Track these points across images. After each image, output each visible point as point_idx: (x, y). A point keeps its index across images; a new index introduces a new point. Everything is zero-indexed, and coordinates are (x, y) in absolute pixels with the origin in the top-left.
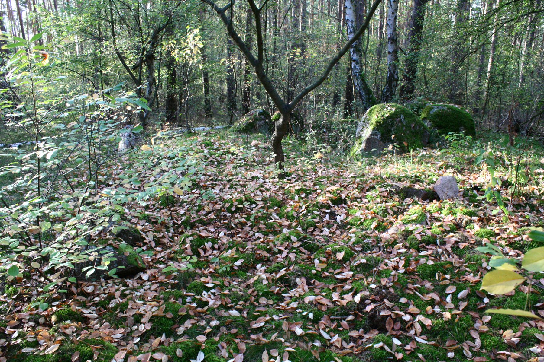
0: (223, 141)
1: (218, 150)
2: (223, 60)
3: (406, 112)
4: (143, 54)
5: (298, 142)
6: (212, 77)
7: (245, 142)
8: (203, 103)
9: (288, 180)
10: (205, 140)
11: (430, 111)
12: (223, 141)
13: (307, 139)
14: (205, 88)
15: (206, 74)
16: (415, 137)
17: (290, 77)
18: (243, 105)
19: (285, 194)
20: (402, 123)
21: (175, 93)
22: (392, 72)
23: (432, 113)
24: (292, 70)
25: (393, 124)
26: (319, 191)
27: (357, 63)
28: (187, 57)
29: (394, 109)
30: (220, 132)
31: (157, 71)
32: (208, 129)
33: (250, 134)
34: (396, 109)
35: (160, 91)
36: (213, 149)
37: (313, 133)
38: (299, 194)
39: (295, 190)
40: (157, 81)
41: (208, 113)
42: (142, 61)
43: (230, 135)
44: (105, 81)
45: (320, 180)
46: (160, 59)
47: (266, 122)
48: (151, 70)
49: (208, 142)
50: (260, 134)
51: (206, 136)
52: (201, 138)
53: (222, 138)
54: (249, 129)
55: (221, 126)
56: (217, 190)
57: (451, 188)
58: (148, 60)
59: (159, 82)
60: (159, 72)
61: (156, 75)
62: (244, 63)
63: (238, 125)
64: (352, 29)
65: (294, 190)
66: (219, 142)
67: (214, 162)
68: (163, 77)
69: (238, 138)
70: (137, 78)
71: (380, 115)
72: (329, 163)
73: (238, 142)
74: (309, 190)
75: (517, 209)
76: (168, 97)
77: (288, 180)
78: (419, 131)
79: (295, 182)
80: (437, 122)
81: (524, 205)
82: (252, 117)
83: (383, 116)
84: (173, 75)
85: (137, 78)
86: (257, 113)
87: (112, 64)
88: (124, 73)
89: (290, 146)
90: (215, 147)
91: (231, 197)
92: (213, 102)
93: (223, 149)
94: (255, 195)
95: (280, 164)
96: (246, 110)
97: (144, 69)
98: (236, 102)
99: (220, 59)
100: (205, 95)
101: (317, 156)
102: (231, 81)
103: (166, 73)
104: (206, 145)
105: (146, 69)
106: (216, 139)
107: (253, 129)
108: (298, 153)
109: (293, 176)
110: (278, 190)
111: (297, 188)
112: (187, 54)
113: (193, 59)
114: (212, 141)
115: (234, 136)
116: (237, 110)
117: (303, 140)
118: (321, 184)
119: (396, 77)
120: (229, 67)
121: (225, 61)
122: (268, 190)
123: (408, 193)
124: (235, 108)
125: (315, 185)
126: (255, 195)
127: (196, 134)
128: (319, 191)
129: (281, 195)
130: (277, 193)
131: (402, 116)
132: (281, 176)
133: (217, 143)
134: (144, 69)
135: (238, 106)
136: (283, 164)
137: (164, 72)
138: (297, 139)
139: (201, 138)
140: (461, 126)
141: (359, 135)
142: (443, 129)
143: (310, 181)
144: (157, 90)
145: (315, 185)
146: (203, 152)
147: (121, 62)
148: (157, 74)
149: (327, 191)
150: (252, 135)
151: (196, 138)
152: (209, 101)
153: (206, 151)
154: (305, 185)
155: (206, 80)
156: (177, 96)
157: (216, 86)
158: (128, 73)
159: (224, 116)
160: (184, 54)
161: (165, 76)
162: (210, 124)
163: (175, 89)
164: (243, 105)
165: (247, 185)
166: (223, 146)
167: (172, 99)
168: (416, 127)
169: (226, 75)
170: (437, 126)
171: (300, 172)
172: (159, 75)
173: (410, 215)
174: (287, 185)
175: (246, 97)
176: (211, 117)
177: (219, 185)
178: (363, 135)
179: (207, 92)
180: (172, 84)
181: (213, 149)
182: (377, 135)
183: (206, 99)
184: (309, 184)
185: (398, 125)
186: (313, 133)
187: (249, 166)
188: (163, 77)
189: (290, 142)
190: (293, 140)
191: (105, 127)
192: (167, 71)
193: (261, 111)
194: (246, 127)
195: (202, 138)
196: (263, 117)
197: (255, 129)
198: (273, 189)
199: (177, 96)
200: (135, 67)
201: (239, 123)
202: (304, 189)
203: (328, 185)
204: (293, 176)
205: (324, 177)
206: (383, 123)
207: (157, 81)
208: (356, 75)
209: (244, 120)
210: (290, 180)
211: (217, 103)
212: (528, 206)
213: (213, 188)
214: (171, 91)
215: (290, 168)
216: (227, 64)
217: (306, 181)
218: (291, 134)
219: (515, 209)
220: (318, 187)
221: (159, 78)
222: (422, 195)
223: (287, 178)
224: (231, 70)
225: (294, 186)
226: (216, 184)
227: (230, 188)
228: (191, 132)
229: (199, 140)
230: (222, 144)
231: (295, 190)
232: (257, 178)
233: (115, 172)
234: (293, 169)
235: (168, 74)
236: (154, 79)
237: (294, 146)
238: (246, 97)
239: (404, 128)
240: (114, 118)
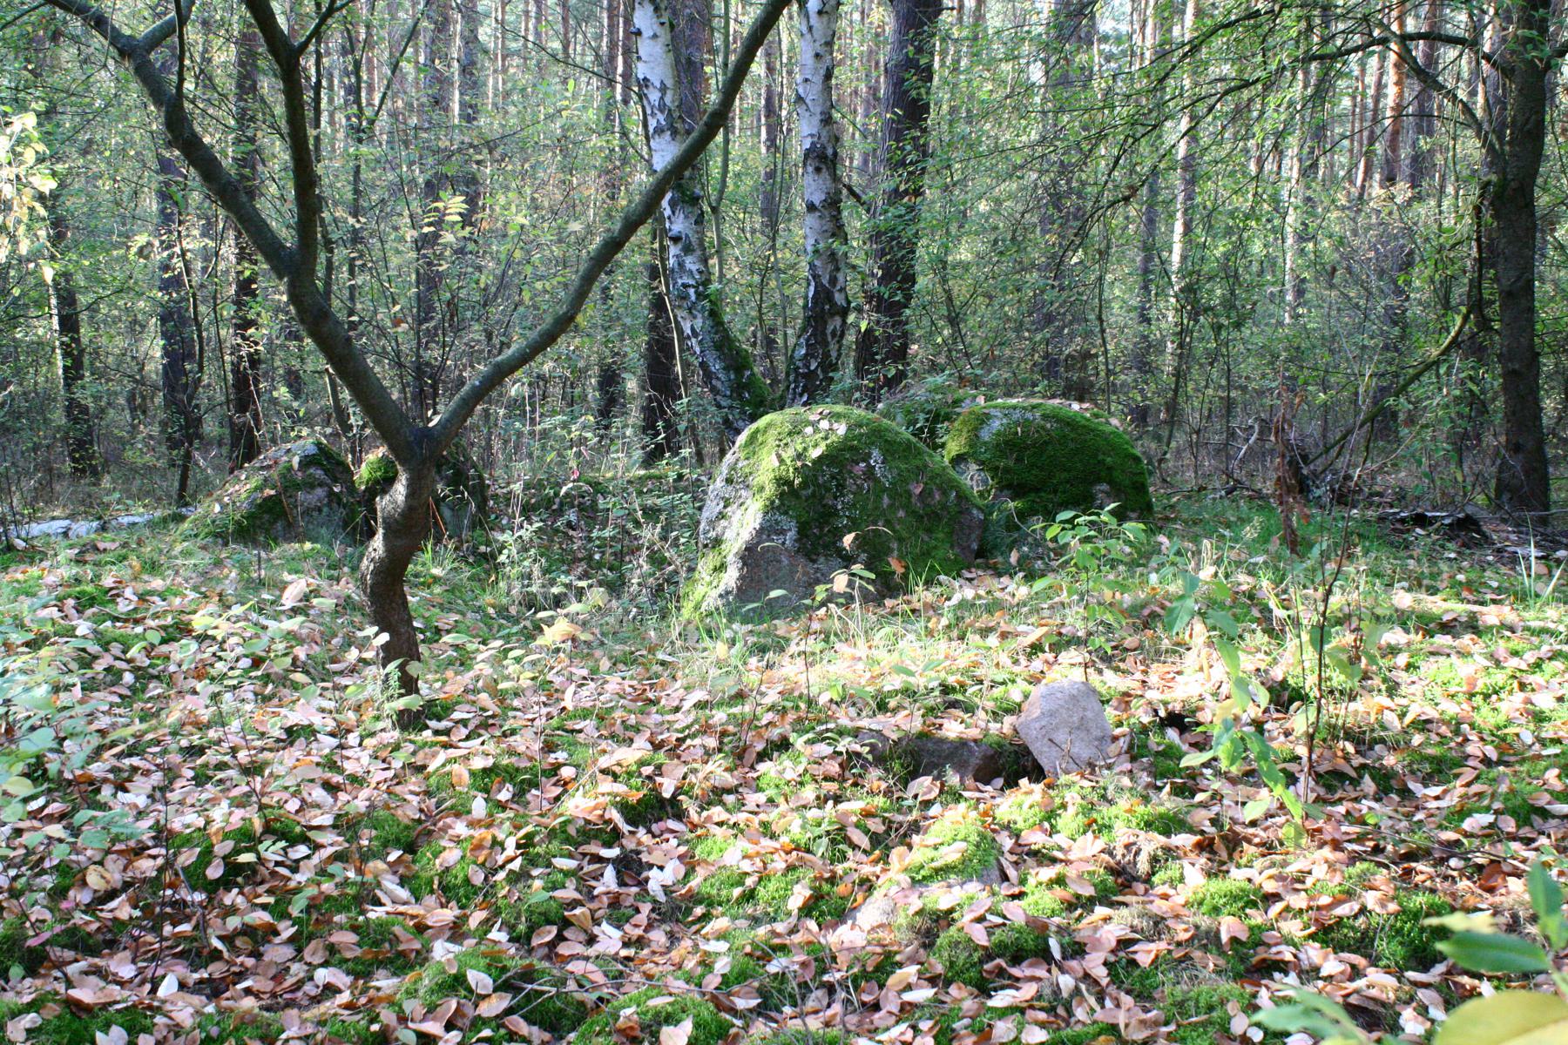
3: (889, 436)
11: (976, 429)
16: (929, 531)
20: (876, 480)
22: (825, 282)
23: (985, 435)
25: (841, 487)
27: (688, 249)
29: (841, 429)
34: (849, 429)
47: (331, 493)
57: (1082, 726)
63: (217, 508)
64: (661, 117)
71: (788, 454)
75: (1330, 789)
78: (944, 507)
80: (1007, 470)
81: (1353, 774)
83: (799, 456)
86: (296, 461)
119: (839, 298)
123: (917, 757)
131: (875, 453)
140: (1099, 480)
141: (712, 534)
142: (1032, 496)
168: (931, 494)
170: (1009, 486)
173: (936, 848)
178: (728, 535)
182: (783, 532)
185: (860, 487)
206: (804, 485)
208: (685, 297)
212: (1367, 778)
219: (1322, 791)
222: (975, 761)
239: (886, 500)
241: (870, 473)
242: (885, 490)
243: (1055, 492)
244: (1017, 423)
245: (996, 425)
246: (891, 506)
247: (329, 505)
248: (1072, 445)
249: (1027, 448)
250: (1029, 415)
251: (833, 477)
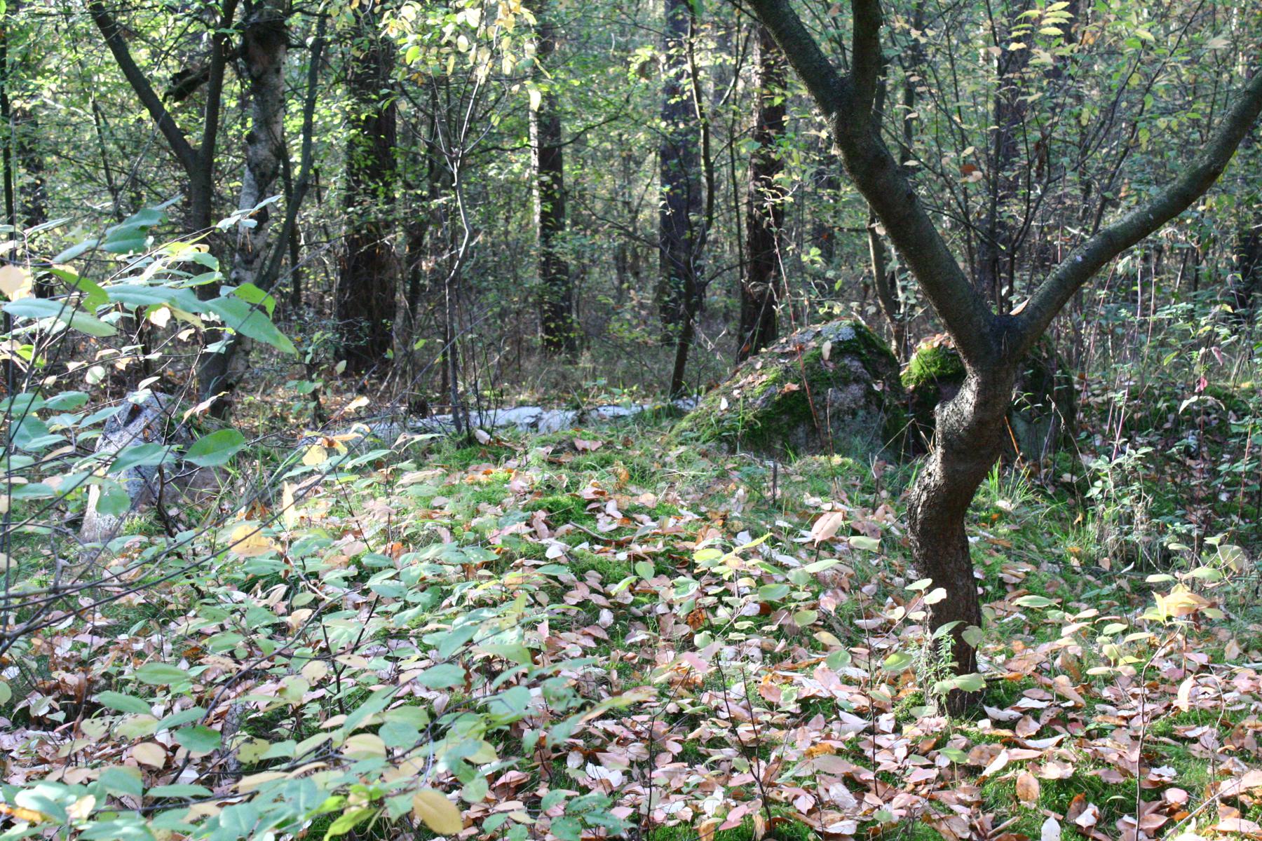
0: (647, 498)
1: (620, 546)
2: (644, 54)
4: (227, 22)
5: (1045, 507)
6: (578, 139)
7: (761, 501)
8: (532, 277)
9: (997, 724)
10: (551, 488)
12: (647, 498)
13: (1094, 492)
14: (545, 198)
15: (550, 125)
17: (1003, 149)
18: (745, 295)
19: (983, 806)
21: (389, 226)
24: (1010, 112)
26: (1174, 796)
28: (463, 43)
30: (626, 443)
31: (295, 106)
32: (558, 418)
33: (784, 458)
35: (309, 213)
36: (594, 540)
37: (1130, 458)
38: (1062, 809)
39: (1044, 784)
40: (296, 158)
41: (559, 326)
42: (221, 53)
43: (682, 461)
44: (22, 150)
45: (1180, 730)
46: (319, 44)
47: (869, 392)
48: (265, 97)
49: (564, 499)
50: (837, 459)
51: (553, 463)
52: (527, 473)
53: (642, 476)
54: (783, 427)
55: (623, 404)
56: (611, 771)
58: (257, 52)
59: (308, 161)
60: (309, 111)
61: (293, 124)
62: (753, 68)
63: (724, 404)
65: (1035, 787)
66: (626, 502)
67: (595, 611)
68: (328, 138)
69: (723, 477)
70: (195, 139)
72: (1223, 633)
73: (723, 499)
74: (1117, 788)
76: (352, 243)
77: (997, 724)
79: (1039, 735)
82: (799, 363)
84: (380, 128)
85: (195, 139)
86: (827, 347)
87: (62, 59)
88: (123, 108)
89: (1003, 529)
90: (604, 526)
91: (688, 814)
92: (584, 270)
93: (643, 540)
94: (820, 805)
95: (956, 633)
96: (759, 326)
97: (232, 87)
98: (704, 283)
99: (626, 49)
100: (546, 237)
101: (1172, 604)
102: (677, 158)
103: (347, 117)
104: (558, 517)
105: (242, 97)
106: (610, 483)
107: (801, 432)
108: (1045, 566)
109: (1025, 703)
110: (944, 782)
111: (1053, 772)
112: (463, 29)
113: (496, 56)
114: (587, 491)
115: (703, 470)
116: (710, 316)
117: (1073, 495)
118: (1188, 757)
120: (672, 89)
121: (654, 60)
122: (889, 779)
124: (699, 306)
125: (1150, 759)
126: (820, 805)
127: (497, 452)
128: (1174, 796)
129: (964, 813)
130: (943, 795)
132: (963, 706)
133: (611, 507)
134: (232, 87)
135: (716, 296)
136: (972, 635)
137: (333, 109)
138: (1041, 490)
139: (527, 473)
143: (1124, 736)
144: (294, 205)
145: (1150, 759)
146: (539, 553)
147: (110, 55)
148: (299, 121)
149: (1227, 801)
150: (797, 464)
151: (499, 472)
152: (563, 268)
153: (555, 549)
154: (1099, 761)
155: (550, 159)
156: (396, 239)
157: (603, 185)
158: (146, 114)
159: (641, 347)
160: (448, 30)
161: (342, 135)
162: (562, 391)
163: (390, 200)
164: (745, 295)
165: (773, 744)
166: (649, 526)
167: (370, 254)
169: (656, 130)
171: (1062, 679)
172: (308, 129)
174: (993, 756)
175: (762, 251)
176: (571, 348)
177: (623, 742)
179: (551, 222)
180: (375, 173)
181: (594, 540)
183: (548, 255)
184: (1120, 750)
186: (1130, 458)
187: (787, 641)
188: (328, 138)
189: (1003, 504)
190: (1020, 496)
191: (39, 429)
192: (347, 104)
193: (847, 333)
194: (764, 417)
195: (537, 476)
196: (856, 365)
197: (814, 431)
198: (920, 775)
199: (396, 239)
200: (183, 87)
201: (727, 394)
202: (1090, 783)
203: (1228, 763)
204: (1025, 703)
205: (1203, 717)
207: (296, 158)
209: (757, 380)
210: (1011, 724)
211: (603, 277)
213: (591, 757)
214: (366, 212)
215: (1010, 655)
216: (666, 75)
217: (1102, 733)
218: (1008, 463)
220: (1167, 773)
221: (307, 146)
223: (993, 711)
224: (684, 109)
225: (1037, 762)
226: (610, 735)
227: (690, 756)
228: (471, 440)
229: (519, 484)
230: (640, 509)
231: (1044, 784)
232: (830, 707)
233: (64, 648)
234: (1027, 658)
235: (353, 124)
236: (281, 152)
237: (1025, 530)
238: (762, 251)
240: (89, 378)
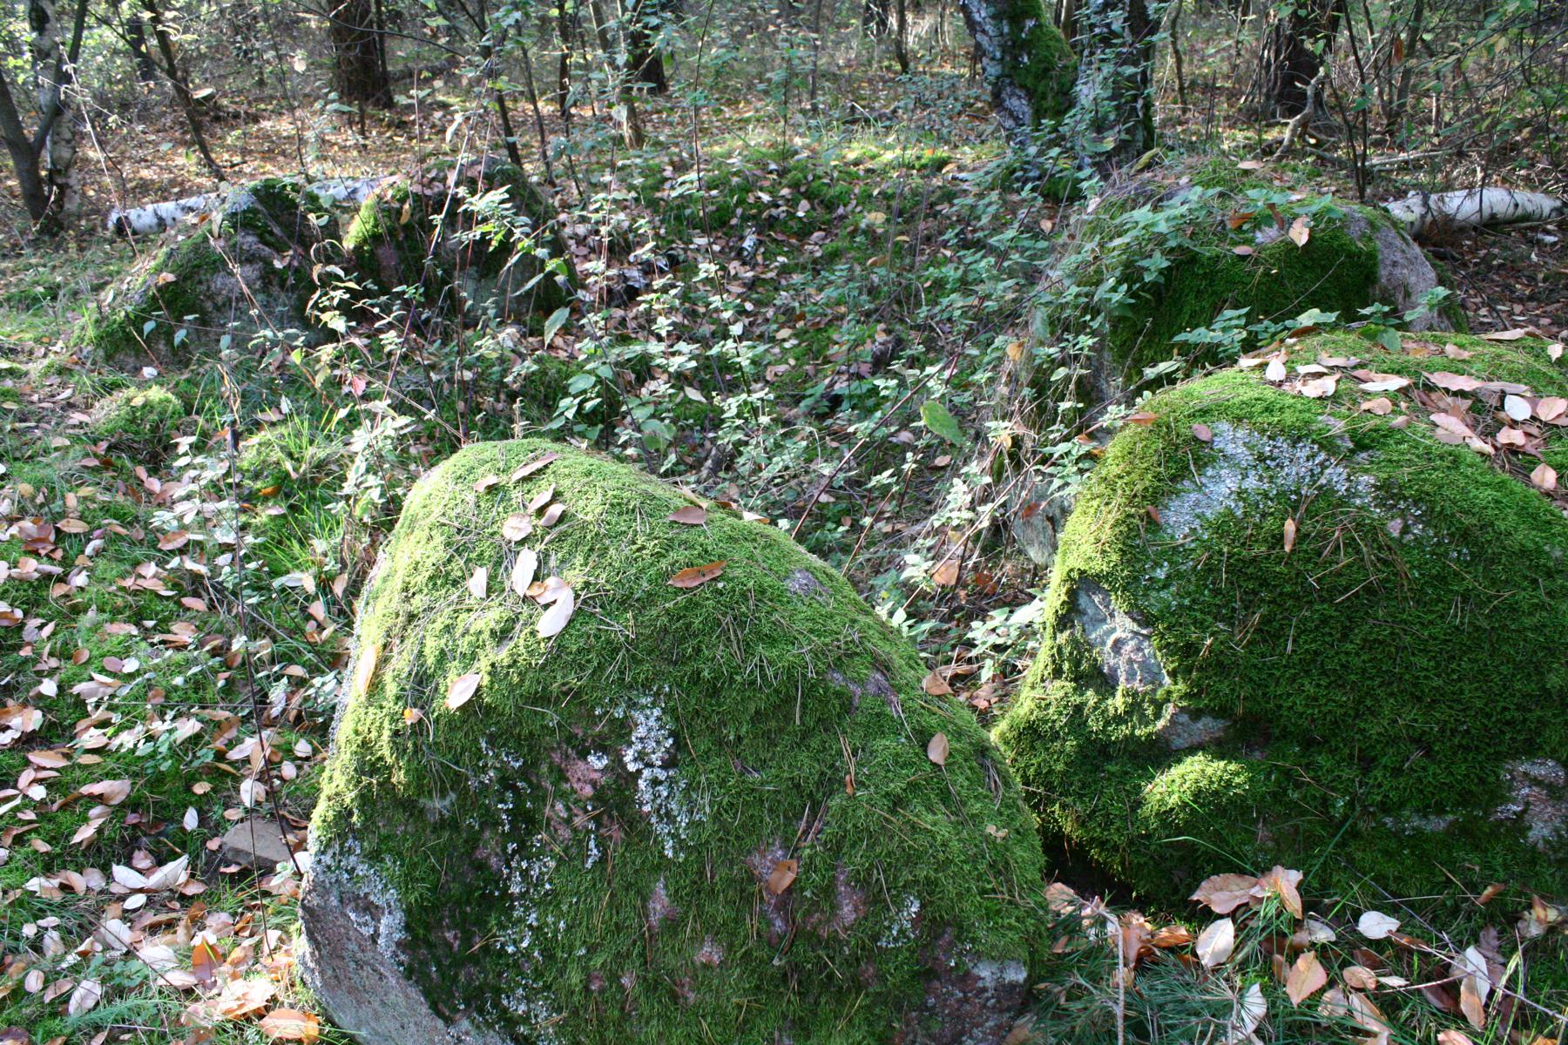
20: (636, 828)
23: (1179, 520)
25: (526, 821)
78: (869, 950)
239: (660, 902)
241: (616, 797)
242: (662, 864)
243: (1367, 763)
244: (1290, 503)
245: (1221, 489)
246: (673, 925)
247: (265, 289)
248: (1456, 616)
249: (1303, 597)
250: (1336, 475)
251: (506, 782)
